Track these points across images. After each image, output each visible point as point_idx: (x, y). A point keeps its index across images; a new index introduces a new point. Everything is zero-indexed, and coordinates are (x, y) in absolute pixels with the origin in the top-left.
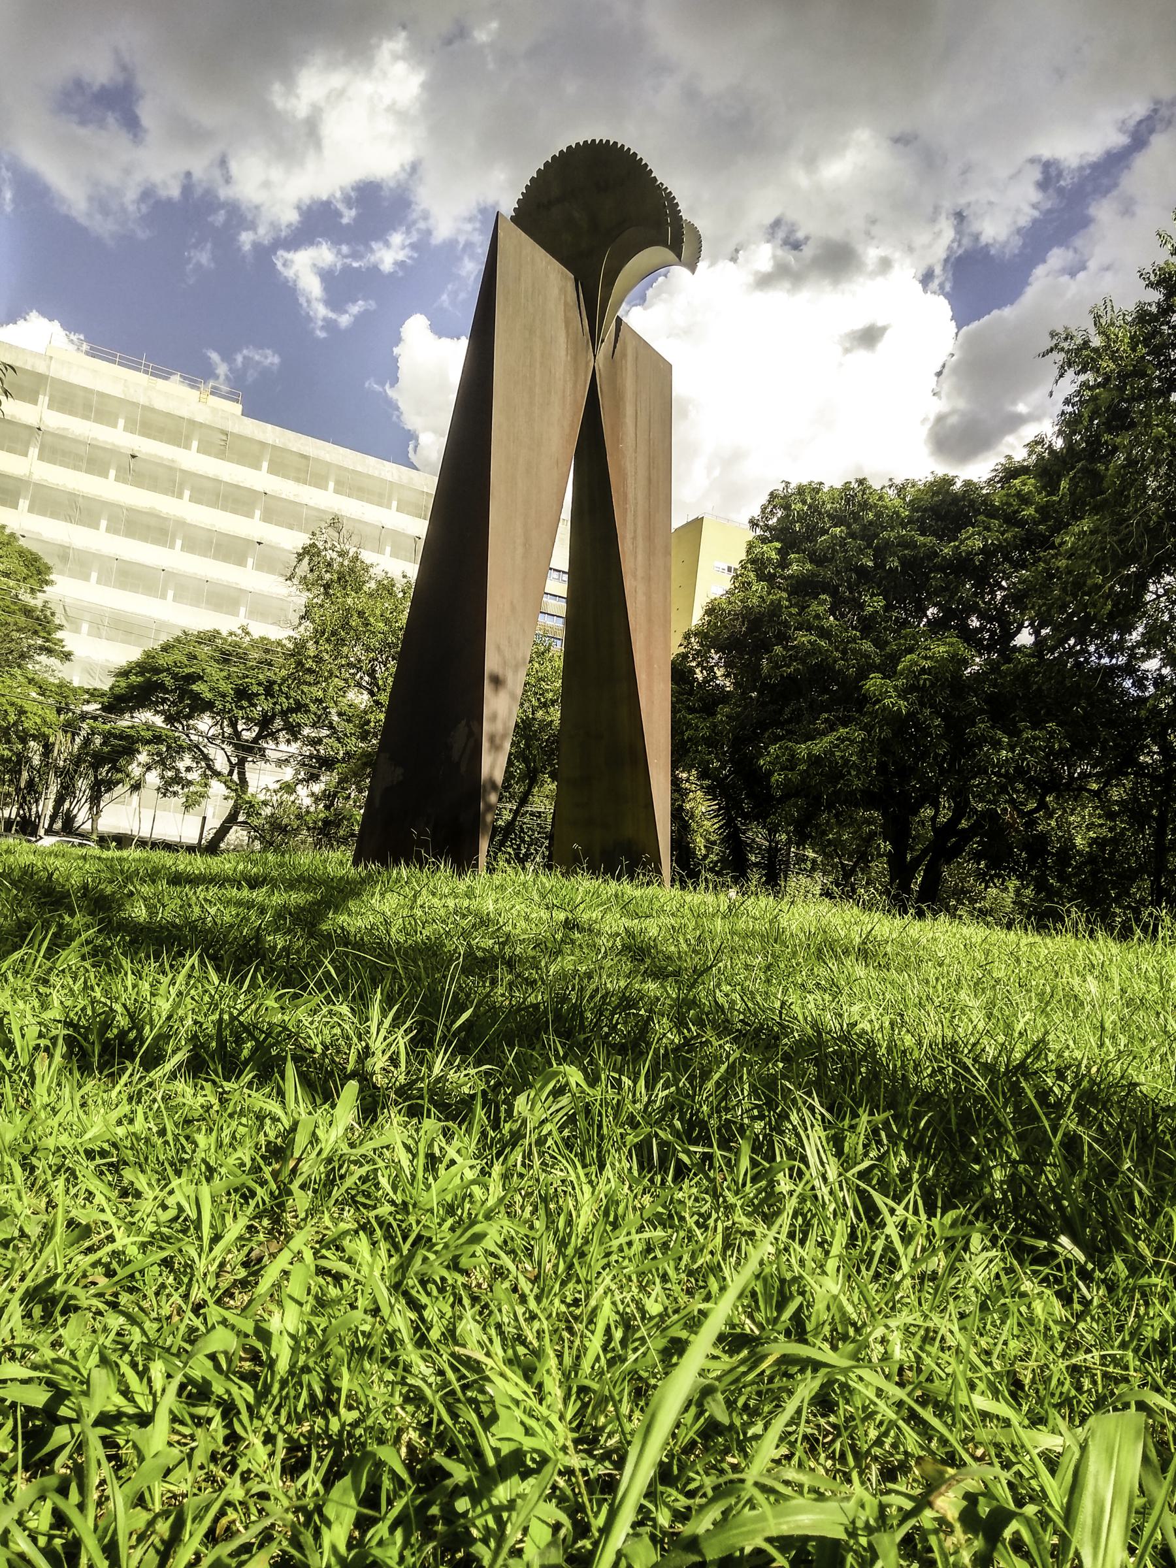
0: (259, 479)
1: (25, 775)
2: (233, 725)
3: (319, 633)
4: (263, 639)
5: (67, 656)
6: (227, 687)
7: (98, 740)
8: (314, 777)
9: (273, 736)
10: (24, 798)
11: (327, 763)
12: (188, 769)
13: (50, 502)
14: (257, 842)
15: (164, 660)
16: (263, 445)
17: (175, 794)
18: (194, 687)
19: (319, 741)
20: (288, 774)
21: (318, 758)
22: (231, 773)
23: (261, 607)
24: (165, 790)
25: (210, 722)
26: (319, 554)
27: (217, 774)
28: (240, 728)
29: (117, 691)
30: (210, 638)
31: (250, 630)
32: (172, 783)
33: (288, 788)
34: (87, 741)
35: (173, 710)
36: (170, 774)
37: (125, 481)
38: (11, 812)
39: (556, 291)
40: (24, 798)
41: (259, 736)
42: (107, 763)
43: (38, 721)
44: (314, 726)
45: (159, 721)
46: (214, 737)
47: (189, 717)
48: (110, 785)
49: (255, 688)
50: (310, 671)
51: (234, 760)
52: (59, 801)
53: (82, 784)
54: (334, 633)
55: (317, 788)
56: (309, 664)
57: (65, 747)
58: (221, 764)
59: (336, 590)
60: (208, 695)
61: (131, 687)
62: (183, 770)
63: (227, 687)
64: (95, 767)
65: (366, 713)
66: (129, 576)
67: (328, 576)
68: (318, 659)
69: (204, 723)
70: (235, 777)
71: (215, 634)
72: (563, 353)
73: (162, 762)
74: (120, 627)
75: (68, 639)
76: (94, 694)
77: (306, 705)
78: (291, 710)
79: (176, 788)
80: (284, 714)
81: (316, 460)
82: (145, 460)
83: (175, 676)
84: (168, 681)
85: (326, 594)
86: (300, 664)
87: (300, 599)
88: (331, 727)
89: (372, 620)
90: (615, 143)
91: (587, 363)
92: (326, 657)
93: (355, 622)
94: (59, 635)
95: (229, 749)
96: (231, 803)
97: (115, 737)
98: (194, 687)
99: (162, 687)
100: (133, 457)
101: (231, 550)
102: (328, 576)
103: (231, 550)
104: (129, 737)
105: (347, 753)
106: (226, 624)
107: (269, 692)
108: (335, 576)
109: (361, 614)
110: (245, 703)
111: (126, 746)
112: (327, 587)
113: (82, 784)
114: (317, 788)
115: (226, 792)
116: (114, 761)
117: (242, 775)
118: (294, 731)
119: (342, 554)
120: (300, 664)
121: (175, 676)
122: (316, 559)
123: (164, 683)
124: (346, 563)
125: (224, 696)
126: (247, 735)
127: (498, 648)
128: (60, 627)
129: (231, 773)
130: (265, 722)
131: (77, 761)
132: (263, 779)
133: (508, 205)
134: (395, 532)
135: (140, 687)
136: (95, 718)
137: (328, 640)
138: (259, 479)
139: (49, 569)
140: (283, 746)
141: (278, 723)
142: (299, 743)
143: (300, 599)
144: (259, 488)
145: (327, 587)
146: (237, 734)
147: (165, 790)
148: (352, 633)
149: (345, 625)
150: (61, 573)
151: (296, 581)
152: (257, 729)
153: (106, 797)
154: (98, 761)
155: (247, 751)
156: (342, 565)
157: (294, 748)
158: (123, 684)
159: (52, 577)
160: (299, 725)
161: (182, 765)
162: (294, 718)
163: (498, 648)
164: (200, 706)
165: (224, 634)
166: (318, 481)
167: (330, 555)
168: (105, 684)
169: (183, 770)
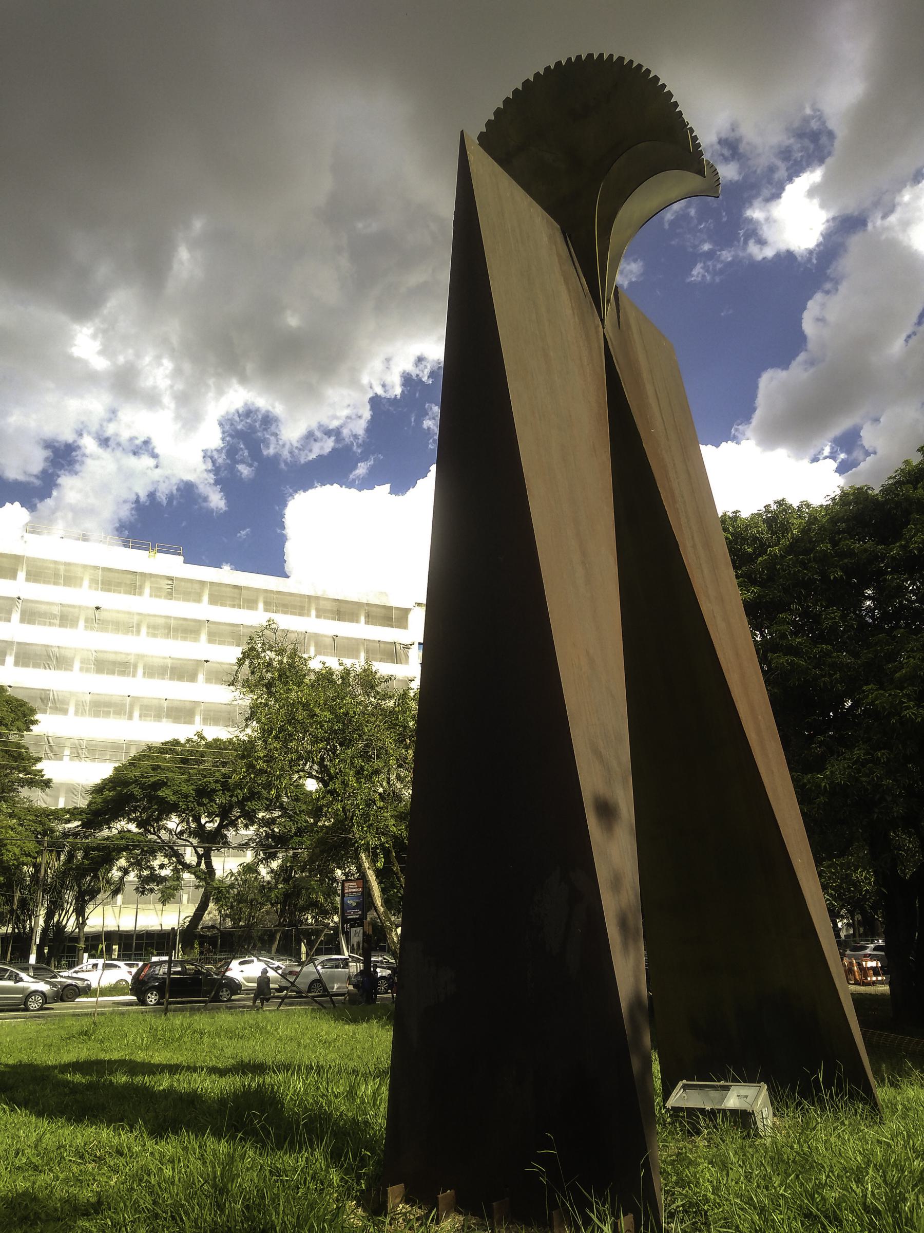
0: (203, 610)
1: (18, 895)
2: (197, 819)
3: (266, 732)
4: (216, 740)
5: (47, 784)
6: (189, 789)
7: (79, 855)
8: (271, 856)
9: (233, 824)
10: (18, 917)
11: (281, 841)
12: (162, 866)
13: (28, 656)
14: (228, 920)
15: (131, 774)
16: (202, 583)
17: (152, 890)
18: (160, 793)
19: (272, 821)
20: (249, 857)
21: (273, 836)
22: (199, 864)
23: (214, 716)
24: (141, 890)
25: (177, 820)
26: (258, 657)
27: (187, 867)
28: (203, 821)
29: (94, 807)
30: (171, 747)
31: (205, 734)
32: (149, 881)
33: (250, 869)
34: (71, 856)
35: (144, 816)
36: (146, 873)
37: (92, 629)
38: (8, 929)
39: (545, 239)
40: (18, 917)
41: (221, 826)
42: (88, 875)
43: (17, 851)
44: (267, 809)
45: (132, 827)
46: (182, 833)
47: (158, 819)
48: (93, 893)
49: (213, 786)
50: (262, 772)
51: (201, 851)
52: (49, 916)
53: (69, 896)
54: (281, 729)
55: (275, 864)
56: (260, 765)
57: (53, 864)
58: (190, 857)
59: (279, 687)
60: (172, 798)
61: (105, 801)
62: (157, 867)
63: (189, 789)
64: (78, 879)
65: (318, 799)
66: (101, 707)
67: (269, 675)
68: (269, 759)
69: (173, 823)
70: (203, 866)
71: (176, 743)
72: (569, 312)
73: (138, 864)
74: (88, 750)
75: (48, 768)
76: (74, 813)
77: (259, 792)
78: (246, 799)
79: (152, 886)
80: (241, 804)
81: (247, 588)
82: (106, 610)
83: (143, 787)
84: (137, 791)
85: (270, 693)
86: (250, 766)
87: (244, 700)
88: (282, 807)
89: (317, 710)
90: (590, 56)
91: (597, 332)
92: (276, 754)
93: (301, 715)
94: (39, 766)
95: (195, 841)
96: (202, 890)
97: (94, 849)
98: (160, 793)
99: (131, 797)
100: (98, 608)
101: (183, 672)
102: (269, 675)
103: (183, 672)
104: (105, 848)
105: (298, 829)
106: (183, 732)
107: (225, 787)
108: (276, 674)
109: (306, 706)
110: (205, 801)
111: (105, 856)
112: (269, 686)
113: (69, 896)
114: (275, 864)
115: (197, 882)
116: (96, 871)
117: (209, 864)
118: (250, 818)
119: (280, 653)
120: (250, 766)
121: (143, 787)
122: (255, 661)
123: (139, 791)
124: (285, 660)
125: (186, 797)
126: (210, 826)
127: (597, 752)
128: (39, 760)
129: (199, 864)
130: (224, 812)
131: (62, 875)
132: (226, 865)
133: (476, 128)
134: (316, 635)
135: (113, 800)
136: (76, 835)
137: (276, 738)
138: (203, 610)
139: (33, 711)
140: (242, 831)
141: (236, 812)
142: (255, 827)
143: (244, 700)
144: (203, 618)
145: (269, 686)
146: (201, 827)
147: (141, 890)
148: (299, 726)
149: (291, 719)
150: (45, 712)
151: (239, 685)
152: (218, 819)
153: (90, 907)
154: (81, 872)
155: (211, 841)
156: (281, 663)
157: (251, 831)
158: (99, 800)
159: (37, 717)
160: (254, 811)
161: (156, 864)
162: (250, 805)
163: (597, 752)
164: (167, 809)
165: (183, 741)
166: (250, 604)
167: (269, 655)
168: (83, 803)
169: (157, 867)
